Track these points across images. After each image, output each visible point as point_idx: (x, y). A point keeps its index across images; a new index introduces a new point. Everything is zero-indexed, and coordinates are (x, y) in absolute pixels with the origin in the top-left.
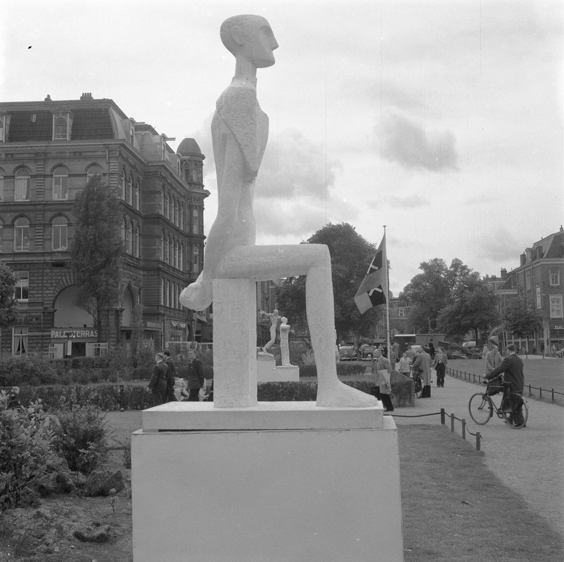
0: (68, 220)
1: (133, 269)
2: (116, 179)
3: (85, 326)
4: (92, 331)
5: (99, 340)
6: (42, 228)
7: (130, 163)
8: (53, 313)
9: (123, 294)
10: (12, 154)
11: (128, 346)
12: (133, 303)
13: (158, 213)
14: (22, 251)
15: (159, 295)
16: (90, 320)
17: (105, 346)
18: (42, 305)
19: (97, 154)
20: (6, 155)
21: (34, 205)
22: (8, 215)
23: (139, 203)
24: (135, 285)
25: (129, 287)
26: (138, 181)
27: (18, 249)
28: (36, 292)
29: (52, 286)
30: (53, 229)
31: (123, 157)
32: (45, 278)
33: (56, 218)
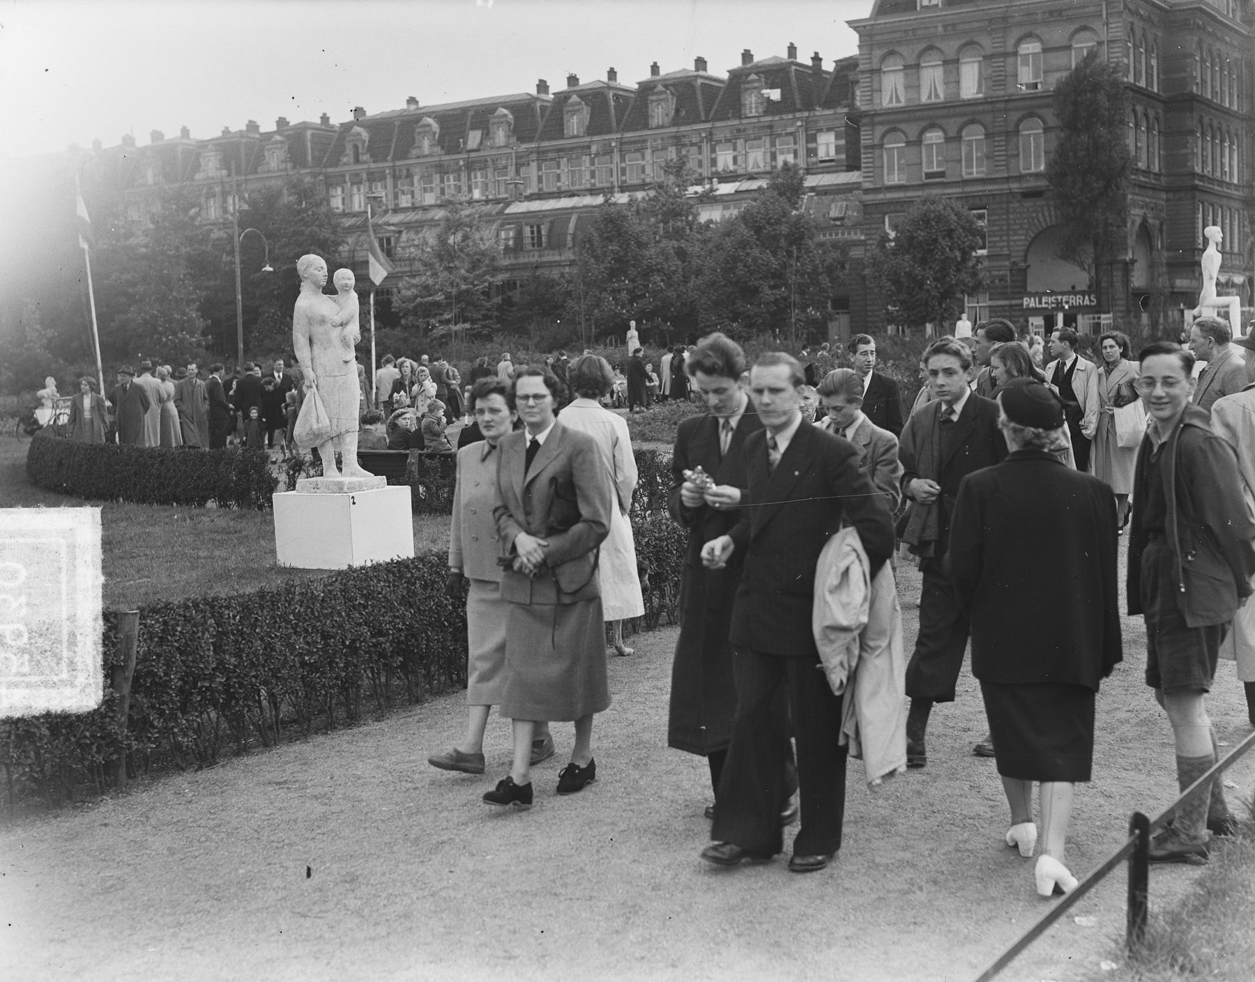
0: (1044, 122)
1: (1151, 193)
2: (1119, 25)
3: (1073, 287)
4: (1087, 297)
5: (1098, 309)
6: (1003, 138)
7: (1141, 16)
8: (1025, 270)
9: (1134, 237)
10: (954, 25)
11: (1145, 318)
12: (1151, 247)
13: (1192, 91)
14: (975, 175)
15: (1194, 233)
16: (1082, 279)
17: (1109, 318)
18: (1009, 259)
19: (1087, 10)
20: (945, 27)
21: (992, 102)
22: (952, 120)
23: (1158, 77)
24: (1154, 218)
25: (1144, 226)
26: (1157, 119)
27: (969, 174)
28: (998, 239)
29: (1022, 228)
30: (1021, 139)
31: (1129, 10)
32: (1011, 216)
33: (1026, 121)
